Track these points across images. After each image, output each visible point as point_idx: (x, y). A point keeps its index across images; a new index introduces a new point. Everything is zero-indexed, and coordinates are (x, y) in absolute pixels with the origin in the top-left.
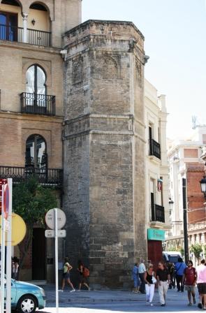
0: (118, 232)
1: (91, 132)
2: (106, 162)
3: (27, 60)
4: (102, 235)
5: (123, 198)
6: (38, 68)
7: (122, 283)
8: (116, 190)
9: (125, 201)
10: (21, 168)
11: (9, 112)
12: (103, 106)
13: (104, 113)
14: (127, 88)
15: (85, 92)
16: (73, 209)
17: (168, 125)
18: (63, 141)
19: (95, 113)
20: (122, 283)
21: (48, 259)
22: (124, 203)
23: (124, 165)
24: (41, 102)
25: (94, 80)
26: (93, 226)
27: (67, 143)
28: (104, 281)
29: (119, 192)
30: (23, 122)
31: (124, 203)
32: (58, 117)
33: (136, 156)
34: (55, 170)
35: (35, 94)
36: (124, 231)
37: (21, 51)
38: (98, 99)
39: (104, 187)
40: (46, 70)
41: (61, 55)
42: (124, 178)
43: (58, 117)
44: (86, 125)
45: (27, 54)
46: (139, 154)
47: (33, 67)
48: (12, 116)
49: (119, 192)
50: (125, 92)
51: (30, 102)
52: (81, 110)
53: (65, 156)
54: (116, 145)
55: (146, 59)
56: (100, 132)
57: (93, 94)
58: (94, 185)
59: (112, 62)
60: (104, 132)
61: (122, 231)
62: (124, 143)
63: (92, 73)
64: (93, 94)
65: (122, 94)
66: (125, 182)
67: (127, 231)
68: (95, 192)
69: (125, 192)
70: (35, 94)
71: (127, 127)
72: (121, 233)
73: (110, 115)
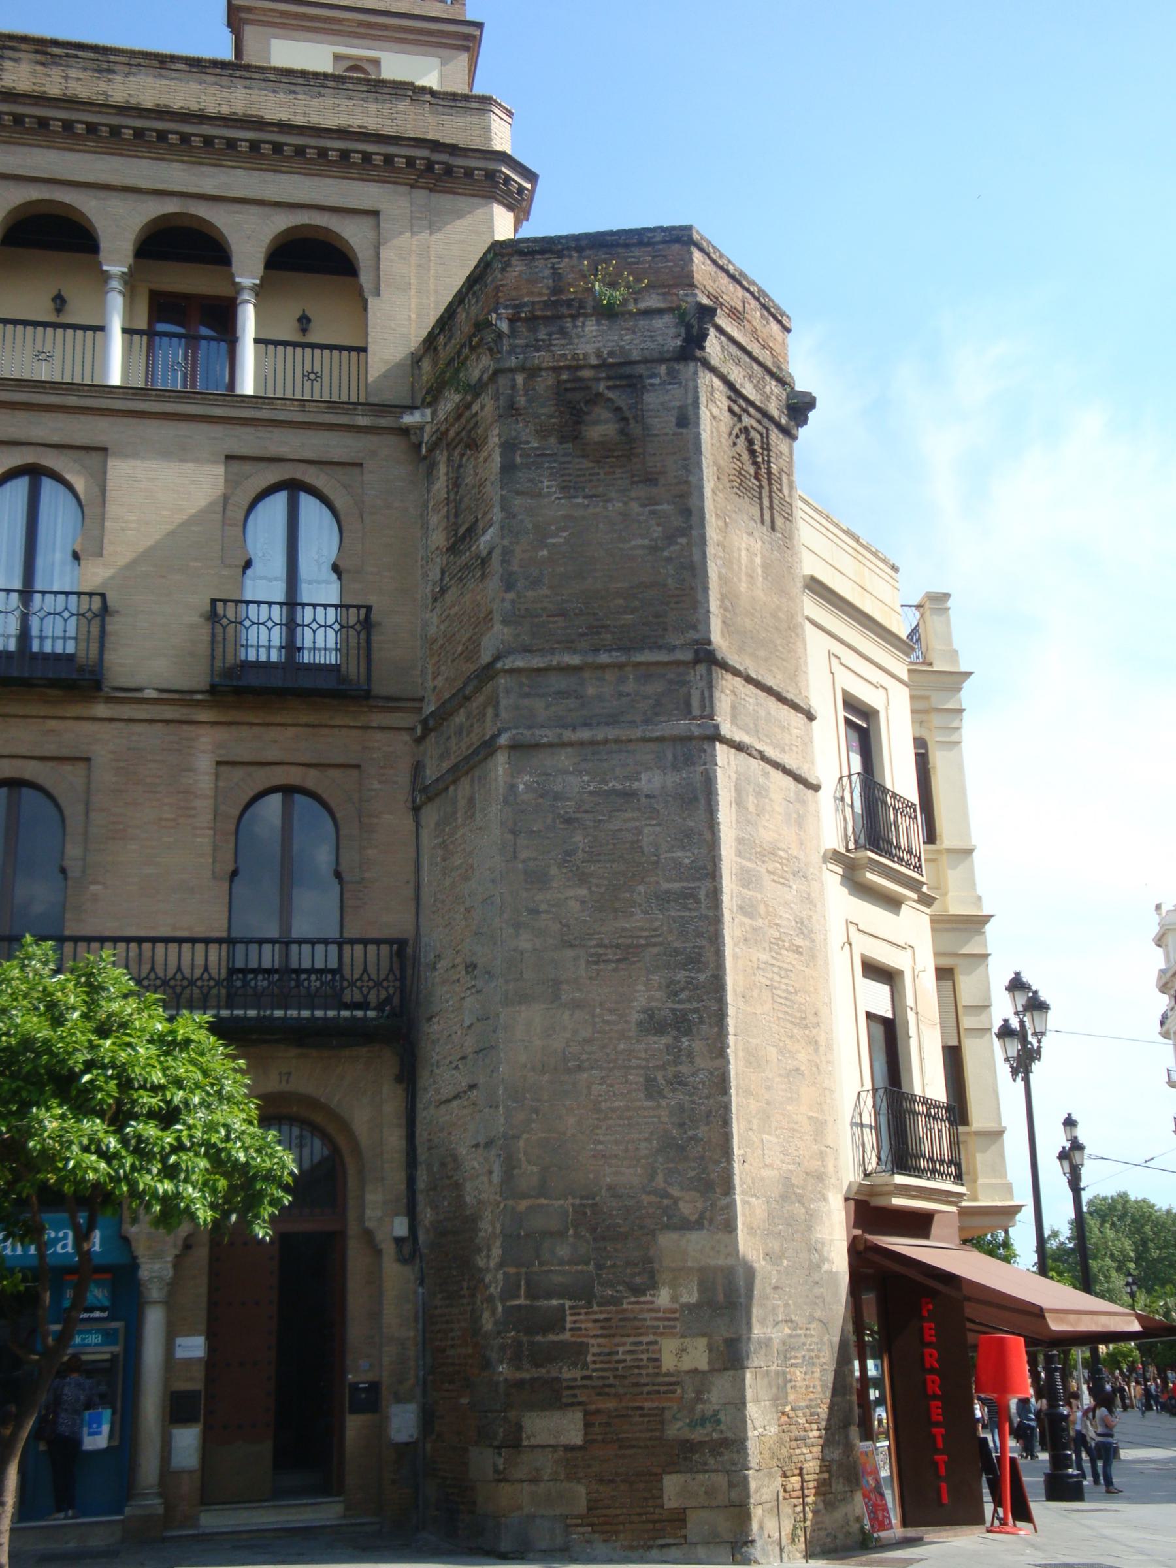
0: (653, 1233)
1: (503, 740)
2: (583, 878)
3: (247, 467)
4: (563, 1251)
5: (675, 1052)
6: (307, 503)
7: (679, 1518)
8: (635, 1017)
9: (684, 1069)
10: (207, 941)
11: (153, 694)
12: (563, 614)
13: (569, 645)
14: (677, 521)
15: (484, 562)
16: (234, 1058)
17: (971, 729)
18: (416, 810)
19: (527, 650)
20: (679, 1518)
21: (354, 1387)
22: (678, 1082)
23: (676, 886)
24: (321, 643)
25: (518, 501)
26: (523, 1205)
27: (430, 816)
28: (581, 1507)
29: (653, 1024)
30: (222, 734)
31: (678, 1082)
32: (392, 703)
33: (740, 841)
34: (378, 942)
35: (292, 603)
36: (686, 1226)
37: (218, 430)
38: (536, 583)
39: (577, 1005)
40: (338, 504)
41: (405, 431)
42: (677, 952)
43: (392, 703)
44: (490, 711)
45: (247, 441)
46: (766, 834)
47: (278, 503)
48: (169, 712)
49: (653, 1024)
50: (670, 539)
51: (262, 641)
52: (471, 651)
53: (425, 876)
54: (629, 795)
55: (800, 408)
56: (547, 735)
57: (515, 567)
58: (523, 998)
59: (606, 415)
60: (568, 735)
61: (667, 1227)
62: (672, 779)
63: (508, 468)
64: (515, 567)
65: (654, 549)
66: (681, 975)
67: (698, 1225)
68: (530, 1034)
69: (681, 1024)
70: (292, 603)
71: (688, 704)
72: (666, 1240)
73: (596, 650)
